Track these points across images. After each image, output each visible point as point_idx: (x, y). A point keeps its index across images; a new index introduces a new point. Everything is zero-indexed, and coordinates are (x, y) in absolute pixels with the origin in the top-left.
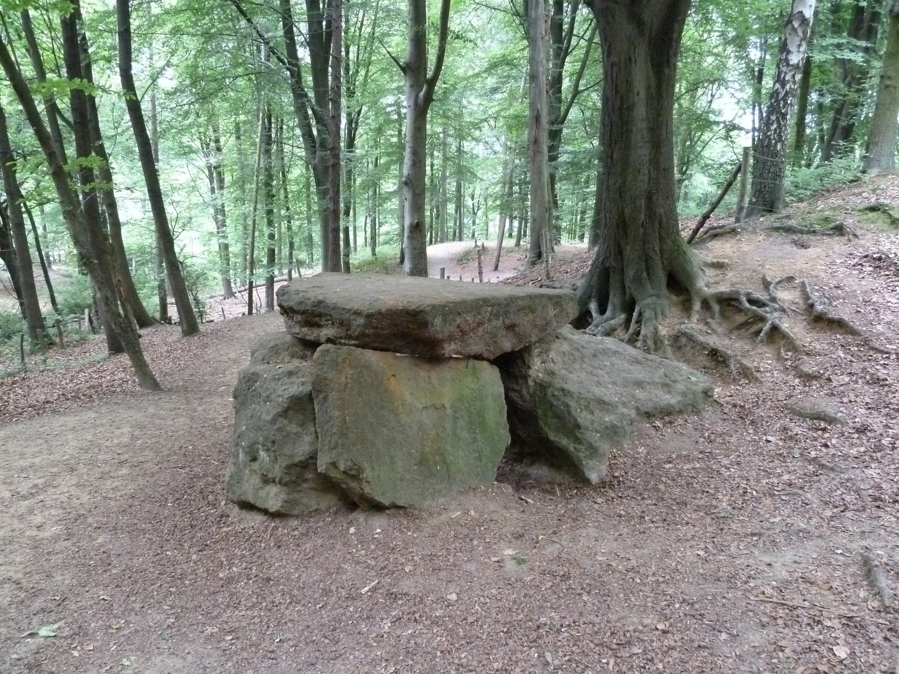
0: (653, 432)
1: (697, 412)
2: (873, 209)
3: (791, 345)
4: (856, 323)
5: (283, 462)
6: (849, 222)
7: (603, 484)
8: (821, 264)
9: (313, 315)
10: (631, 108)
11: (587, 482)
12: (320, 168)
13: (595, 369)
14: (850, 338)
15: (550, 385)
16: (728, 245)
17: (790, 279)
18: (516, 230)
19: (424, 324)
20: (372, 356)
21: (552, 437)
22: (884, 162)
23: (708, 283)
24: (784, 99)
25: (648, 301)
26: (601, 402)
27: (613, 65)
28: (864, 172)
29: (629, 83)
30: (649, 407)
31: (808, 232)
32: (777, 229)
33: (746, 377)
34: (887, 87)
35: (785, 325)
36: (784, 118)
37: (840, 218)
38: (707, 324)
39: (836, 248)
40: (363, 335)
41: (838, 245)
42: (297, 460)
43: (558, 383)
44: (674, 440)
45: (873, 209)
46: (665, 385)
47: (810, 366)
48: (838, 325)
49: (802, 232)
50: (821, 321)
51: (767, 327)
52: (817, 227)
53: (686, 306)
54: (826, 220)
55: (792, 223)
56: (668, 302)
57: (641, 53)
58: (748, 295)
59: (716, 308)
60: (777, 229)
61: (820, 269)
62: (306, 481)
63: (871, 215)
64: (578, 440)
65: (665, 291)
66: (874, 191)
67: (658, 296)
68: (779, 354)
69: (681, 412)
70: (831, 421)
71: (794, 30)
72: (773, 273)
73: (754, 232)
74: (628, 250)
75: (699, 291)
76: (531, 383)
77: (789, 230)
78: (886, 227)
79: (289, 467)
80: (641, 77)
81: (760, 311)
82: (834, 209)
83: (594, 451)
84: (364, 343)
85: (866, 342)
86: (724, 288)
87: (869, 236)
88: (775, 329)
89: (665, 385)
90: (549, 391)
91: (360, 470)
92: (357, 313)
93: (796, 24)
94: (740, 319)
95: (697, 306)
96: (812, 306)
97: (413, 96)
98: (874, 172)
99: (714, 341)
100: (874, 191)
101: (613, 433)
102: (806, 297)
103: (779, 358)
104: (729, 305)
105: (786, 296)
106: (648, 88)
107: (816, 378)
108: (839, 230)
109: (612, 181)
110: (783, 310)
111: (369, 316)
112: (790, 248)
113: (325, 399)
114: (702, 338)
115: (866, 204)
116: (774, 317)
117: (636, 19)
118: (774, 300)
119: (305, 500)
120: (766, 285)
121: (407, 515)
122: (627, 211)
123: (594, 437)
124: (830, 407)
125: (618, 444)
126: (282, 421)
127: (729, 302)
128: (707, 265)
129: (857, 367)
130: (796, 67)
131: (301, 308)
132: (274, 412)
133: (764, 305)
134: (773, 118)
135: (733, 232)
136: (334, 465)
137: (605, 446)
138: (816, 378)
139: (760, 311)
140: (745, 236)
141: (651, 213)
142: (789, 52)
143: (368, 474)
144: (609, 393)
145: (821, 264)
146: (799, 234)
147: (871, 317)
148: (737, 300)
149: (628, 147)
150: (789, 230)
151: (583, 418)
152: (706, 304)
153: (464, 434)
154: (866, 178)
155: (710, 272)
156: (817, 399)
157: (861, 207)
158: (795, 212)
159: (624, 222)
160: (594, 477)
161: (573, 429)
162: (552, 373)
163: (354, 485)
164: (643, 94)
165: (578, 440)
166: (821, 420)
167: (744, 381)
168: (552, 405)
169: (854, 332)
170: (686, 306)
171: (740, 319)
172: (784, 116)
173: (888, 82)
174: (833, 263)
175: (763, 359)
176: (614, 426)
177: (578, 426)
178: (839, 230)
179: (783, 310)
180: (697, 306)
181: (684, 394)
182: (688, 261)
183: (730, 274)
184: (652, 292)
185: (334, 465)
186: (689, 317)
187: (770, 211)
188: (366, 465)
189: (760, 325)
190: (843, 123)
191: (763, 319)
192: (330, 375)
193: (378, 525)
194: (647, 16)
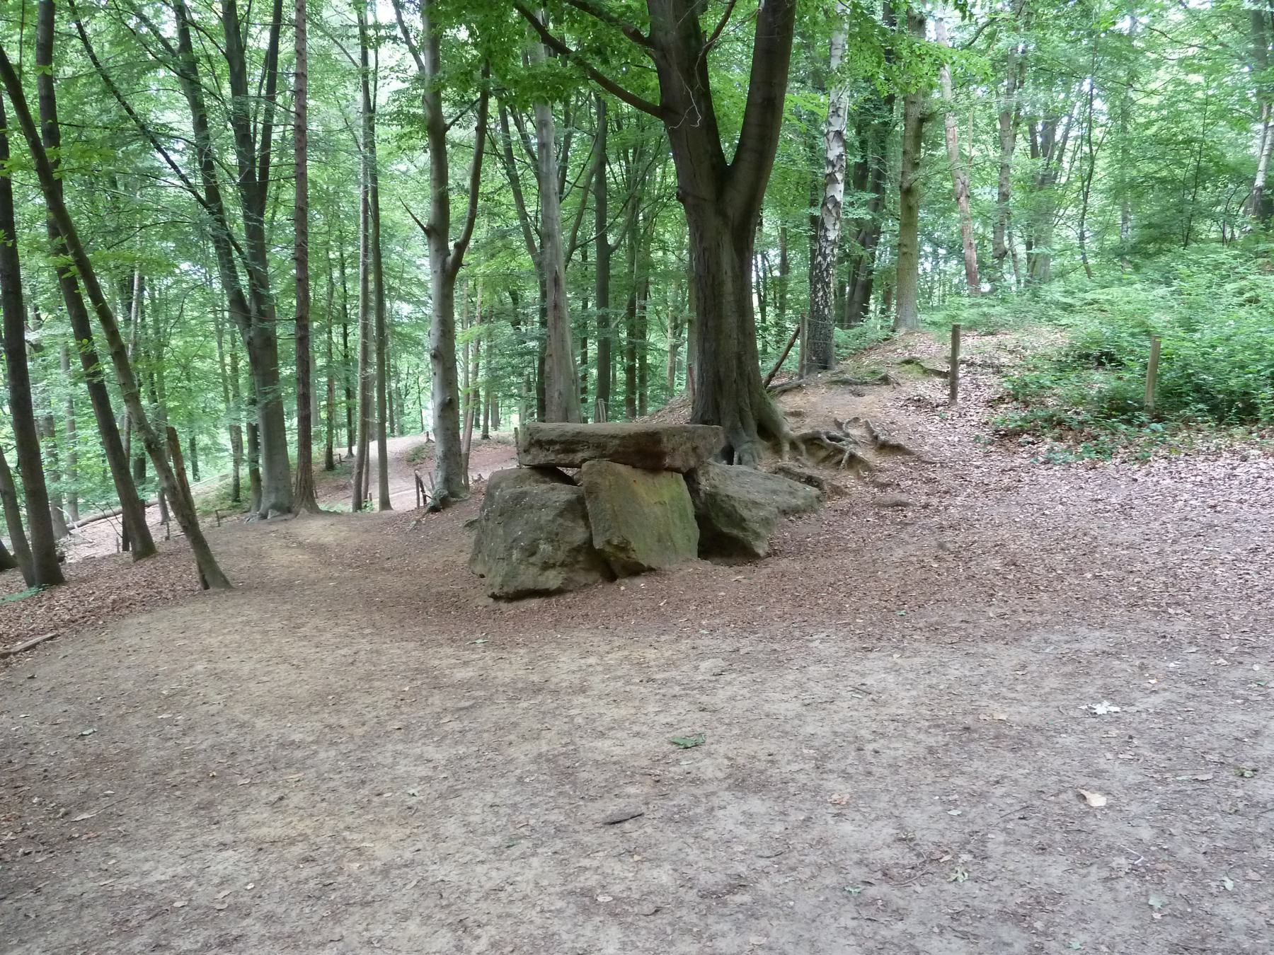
0: (790, 524)
1: (815, 511)
2: (908, 362)
3: (869, 468)
4: (910, 446)
5: (565, 548)
6: (892, 373)
7: (769, 555)
8: (875, 406)
9: (572, 443)
10: (721, 284)
11: (757, 556)
12: (257, 342)
13: (750, 483)
14: (907, 458)
15: (717, 494)
16: (797, 399)
17: (856, 419)
18: (246, 445)
19: (659, 442)
20: (620, 468)
21: (725, 530)
22: (909, 321)
23: (791, 428)
24: (827, 270)
25: (745, 446)
26: (755, 503)
27: (704, 249)
28: (894, 331)
29: (718, 264)
30: (784, 506)
31: (862, 384)
32: (836, 382)
33: (837, 494)
34: (905, 254)
35: (860, 453)
36: (828, 287)
37: (884, 371)
38: (797, 460)
39: (885, 394)
40: (617, 452)
41: (886, 392)
42: (576, 544)
43: (722, 492)
44: (805, 528)
45: (908, 362)
46: (791, 493)
47: (883, 478)
48: (898, 449)
49: (856, 384)
50: (885, 448)
51: (846, 456)
52: (868, 379)
53: (777, 449)
54: (873, 372)
55: (847, 376)
56: (761, 446)
57: (726, 239)
58: (827, 433)
59: (803, 447)
60: (836, 382)
61: (876, 410)
62: (578, 562)
63: (907, 367)
64: (744, 529)
65: (757, 437)
66: (906, 347)
67: (752, 442)
68: (858, 474)
69: (804, 511)
70: (906, 505)
71: (830, 211)
72: (842, 416)
73: (817, 386)
74: (724, 404)
75: (786, 436)
76: (702, 495)
77: (846, 383)
78: (920, 376)
79: (569, 551)
80: (727, 258)
81: (839, 445)
82: (878, 364)
83: (757, 536)
84: (617, 457)
85: (919, 458)
86: (806, 430)
87: (908, 384)
88: (853, 457)
89: (791, 493)
90: (718, 498)
91: (628, 543)
92: (614, 437)
93: (830, 206)
94: (822, 454)
95: (787, 447)
96: (876, 437)
97: (440, 259)
98: (902, 331)
99: (807, 471)
100: (906, 347)
101: (766, 522)
102: (871, 431)
103: (859, 478)
104: (813, 444)
105: (855, 432)
106: (733, 268)
107: (888, 485)
108: (885, 380)
109: (707, 345)
110: (856, 443)
111: (624, 438)
112: (849, 397)
113: (596, 498)
114: (798, 470)
115: (902, 358)
116: (850, 448)
117: (721, 213)
118: (848, 435)
119: (577, 578)
120: (839, 425)
121: (657, 575)
122: (722, 370)
123: (756, 527)
124: (904, 498)
125: (770, 531)
126: (560, 520)
127: (812, 441)
128: (786, 414)
129: (915, 475)
130: (834, 242)
131: (562, 439)
132: (553, 513)
133: (841, 440)
134: (819, 286)
135: (799, 387)
136: (609, 542)
137: (763, 531)
138: (888, 485)
139: (839, 445)
140: (810, 391)
141: (741, 374)
142: (826, 230)
143: (633, 545)
144: (758, 497)
145: (875, 406)
146: (855, 386)
147: (920, 441)
148: (819, 439)
149: (720, 316)
150: (846, 383)
151: (745, 513)
152: (794, 445)
153: (678, 522)
154: (896, 336)
155: (791, 420)
156: (892, 495)
157: (899, 361)
158: (847, 367)
159: (719, 380)
160: (761, 552)
161: (740, 522)
162: (715, 487)
163: (622, 555)
164: (729, 273)
165: (744, 529)
166: (899, 505)
167: (836, 497)
168: (722, 508)
169: (909, 453)
170: (777, 449)
171: (822, 454)
172: (828, 284)
173: (905, 250)
174: (885, 406)
175: (848, 479)
176: (767, 519)
177: (744, 520)
178: (885, 380)
179: (856, 443)
180: (787, 447)
181: (805, 498)
182: (774, 412)
183: (808, 420)
184: (747, 439)
185: (609, 542)
186: (781, 457)
187: (825, 368)
188: (631, 539)
189: (840, 456)
190: (862, 278)
191: (841, 451)
192: (599, 481)
193: (641, 582)
194: (730, 212)
